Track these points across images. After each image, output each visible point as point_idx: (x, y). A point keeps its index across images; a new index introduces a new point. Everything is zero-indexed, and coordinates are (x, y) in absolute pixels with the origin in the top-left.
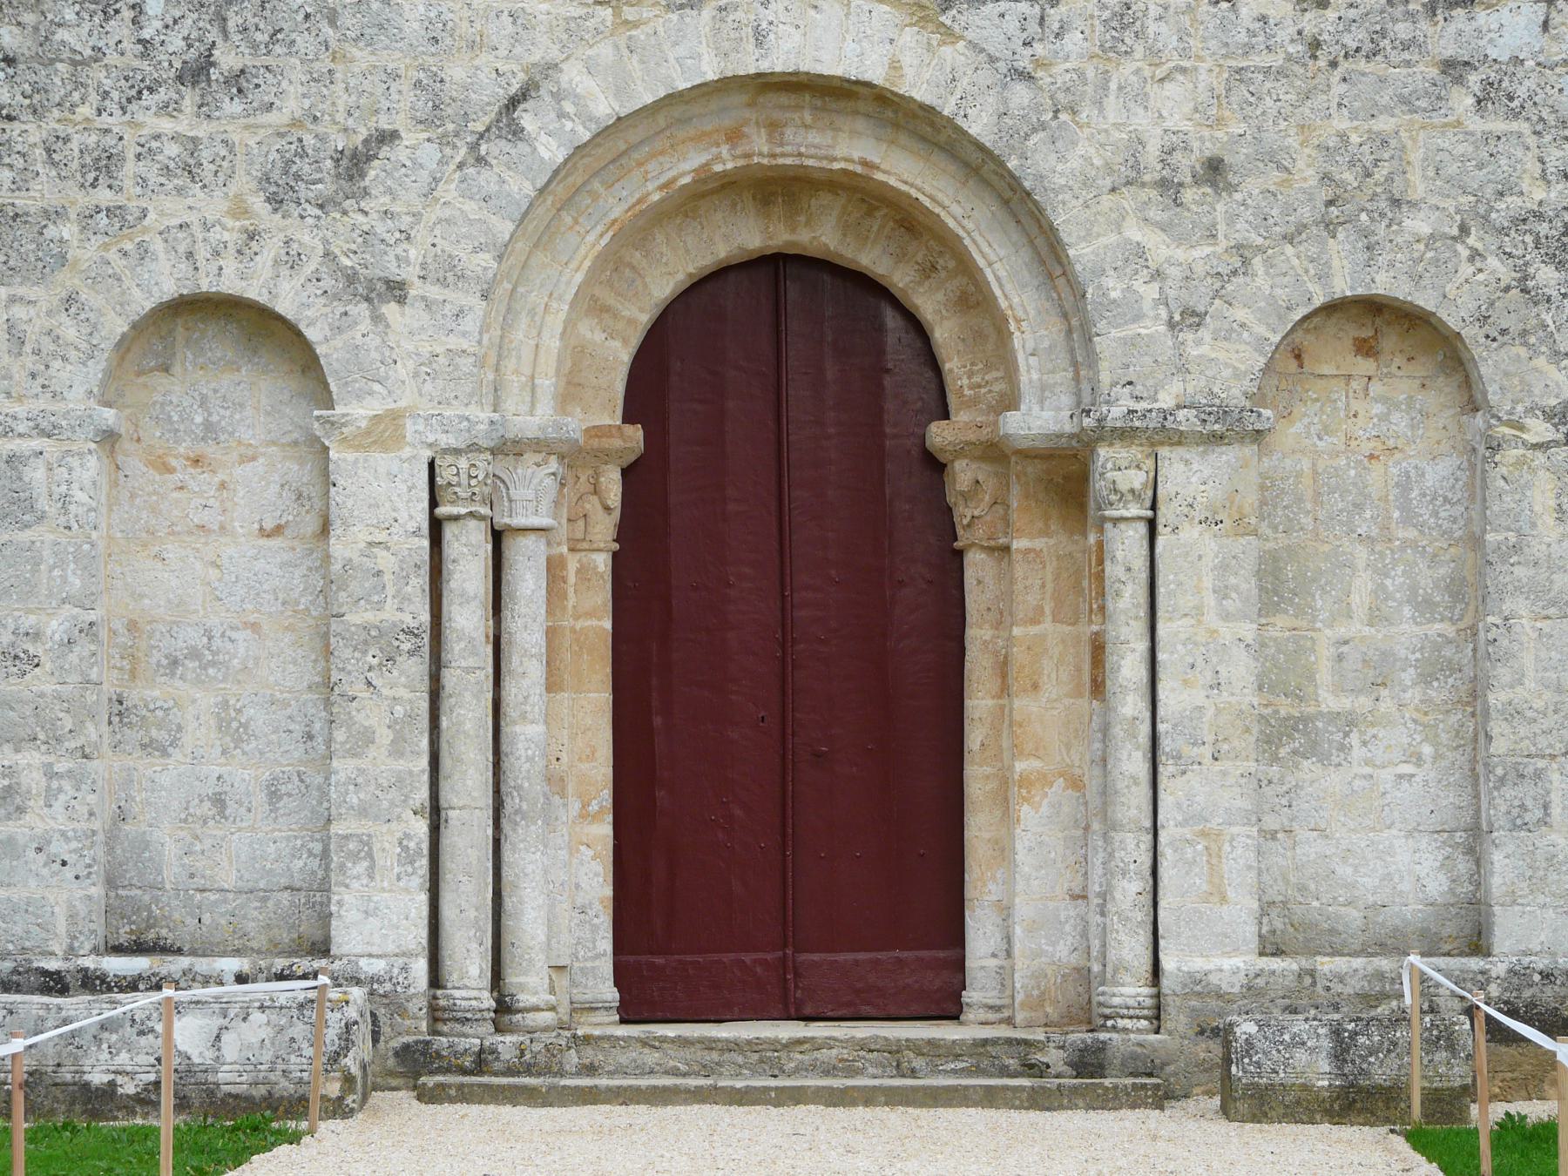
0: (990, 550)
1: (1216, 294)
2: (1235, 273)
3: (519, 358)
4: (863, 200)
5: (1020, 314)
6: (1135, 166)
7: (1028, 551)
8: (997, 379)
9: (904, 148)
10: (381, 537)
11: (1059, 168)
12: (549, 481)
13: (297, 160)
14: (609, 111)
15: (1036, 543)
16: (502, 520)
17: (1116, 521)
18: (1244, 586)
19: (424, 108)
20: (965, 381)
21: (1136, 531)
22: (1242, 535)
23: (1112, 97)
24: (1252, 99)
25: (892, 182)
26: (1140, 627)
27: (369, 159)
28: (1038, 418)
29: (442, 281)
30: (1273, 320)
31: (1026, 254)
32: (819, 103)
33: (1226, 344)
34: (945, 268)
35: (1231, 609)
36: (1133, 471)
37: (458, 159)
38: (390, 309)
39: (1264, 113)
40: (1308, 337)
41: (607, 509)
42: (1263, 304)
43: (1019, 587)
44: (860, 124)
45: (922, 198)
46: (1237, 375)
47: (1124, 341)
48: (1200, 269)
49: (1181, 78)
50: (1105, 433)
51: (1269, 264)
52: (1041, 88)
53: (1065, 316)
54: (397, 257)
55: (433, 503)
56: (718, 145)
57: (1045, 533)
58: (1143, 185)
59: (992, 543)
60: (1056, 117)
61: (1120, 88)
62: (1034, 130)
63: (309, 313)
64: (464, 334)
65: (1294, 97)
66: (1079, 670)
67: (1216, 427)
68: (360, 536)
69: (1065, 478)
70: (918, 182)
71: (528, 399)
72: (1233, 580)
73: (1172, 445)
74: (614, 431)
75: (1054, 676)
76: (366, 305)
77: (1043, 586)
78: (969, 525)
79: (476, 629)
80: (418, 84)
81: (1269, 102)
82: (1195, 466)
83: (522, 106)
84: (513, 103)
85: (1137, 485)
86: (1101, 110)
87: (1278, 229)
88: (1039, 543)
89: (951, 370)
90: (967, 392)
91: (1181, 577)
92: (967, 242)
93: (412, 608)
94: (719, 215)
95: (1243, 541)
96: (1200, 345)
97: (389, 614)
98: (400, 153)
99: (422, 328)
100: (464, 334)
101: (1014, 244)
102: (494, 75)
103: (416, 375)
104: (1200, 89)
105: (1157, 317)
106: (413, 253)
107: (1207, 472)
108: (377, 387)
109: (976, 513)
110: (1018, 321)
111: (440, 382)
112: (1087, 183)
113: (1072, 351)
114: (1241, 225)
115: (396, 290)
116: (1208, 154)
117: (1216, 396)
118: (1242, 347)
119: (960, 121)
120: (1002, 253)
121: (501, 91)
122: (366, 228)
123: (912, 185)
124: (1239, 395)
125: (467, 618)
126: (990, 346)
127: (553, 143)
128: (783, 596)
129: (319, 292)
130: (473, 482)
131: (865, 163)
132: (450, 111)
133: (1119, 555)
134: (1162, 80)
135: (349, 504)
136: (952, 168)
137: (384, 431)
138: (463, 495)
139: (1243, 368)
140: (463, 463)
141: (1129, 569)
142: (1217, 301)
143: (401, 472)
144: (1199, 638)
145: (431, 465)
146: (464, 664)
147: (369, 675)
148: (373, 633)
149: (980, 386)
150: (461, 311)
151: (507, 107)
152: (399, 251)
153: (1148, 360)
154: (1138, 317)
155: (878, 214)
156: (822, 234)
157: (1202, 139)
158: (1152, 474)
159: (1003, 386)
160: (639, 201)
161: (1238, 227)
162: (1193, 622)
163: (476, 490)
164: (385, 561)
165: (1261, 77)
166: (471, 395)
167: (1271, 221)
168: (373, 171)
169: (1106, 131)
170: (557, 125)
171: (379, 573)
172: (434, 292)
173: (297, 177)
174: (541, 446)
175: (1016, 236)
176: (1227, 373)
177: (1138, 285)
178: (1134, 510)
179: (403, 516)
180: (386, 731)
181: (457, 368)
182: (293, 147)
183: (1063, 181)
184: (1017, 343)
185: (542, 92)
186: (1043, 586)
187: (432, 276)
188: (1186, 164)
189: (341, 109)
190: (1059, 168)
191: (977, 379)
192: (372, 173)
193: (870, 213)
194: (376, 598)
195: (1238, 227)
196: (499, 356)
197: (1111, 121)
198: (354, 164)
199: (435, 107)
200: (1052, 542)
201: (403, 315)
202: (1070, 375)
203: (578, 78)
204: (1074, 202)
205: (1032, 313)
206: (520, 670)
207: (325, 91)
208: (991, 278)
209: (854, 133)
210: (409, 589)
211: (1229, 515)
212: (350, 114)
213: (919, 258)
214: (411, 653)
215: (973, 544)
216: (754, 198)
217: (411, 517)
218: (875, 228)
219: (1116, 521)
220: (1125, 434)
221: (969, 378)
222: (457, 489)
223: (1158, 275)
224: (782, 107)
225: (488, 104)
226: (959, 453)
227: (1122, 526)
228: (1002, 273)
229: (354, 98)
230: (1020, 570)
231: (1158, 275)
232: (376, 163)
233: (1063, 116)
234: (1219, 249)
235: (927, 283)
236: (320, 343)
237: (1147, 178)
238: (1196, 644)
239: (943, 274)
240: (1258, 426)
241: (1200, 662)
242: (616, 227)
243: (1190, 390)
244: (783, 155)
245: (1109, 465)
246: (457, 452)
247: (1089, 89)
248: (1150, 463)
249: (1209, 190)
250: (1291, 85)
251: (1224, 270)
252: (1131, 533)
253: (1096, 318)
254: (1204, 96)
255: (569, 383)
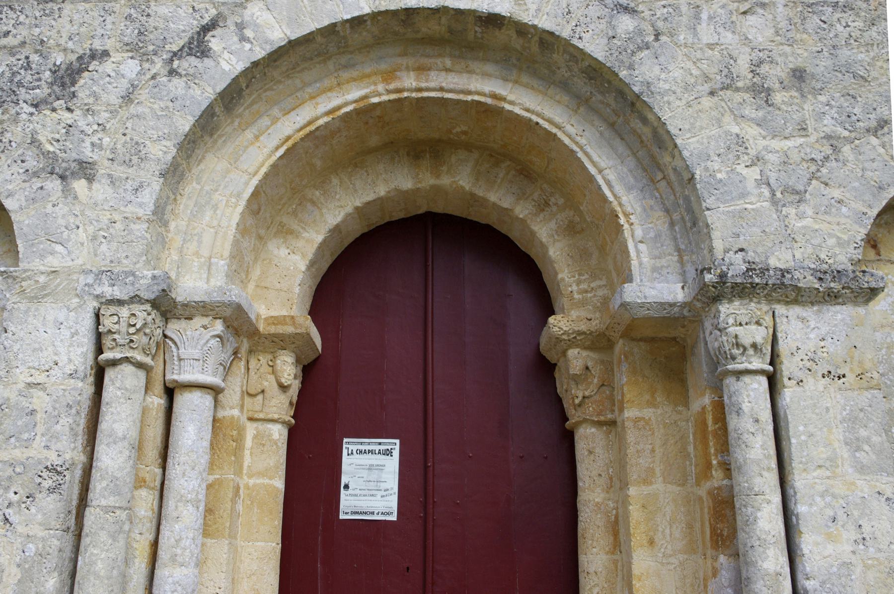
0: (600, 424)
1: (813, 176)
2: (827, 158)
3: (200, 242)
4: (491, 156)
5: (629, 209)
6: (730, 74)
7: (637, 420)
8: (600, 287)
9: (526, 86)
10: (40, 378)
11: (663, 76)
12: (214, 342)
13: (22, 72)
14: (282, 35)
15: (647, 417)
16: (174, 376)
17: (739, 374)
18: (876, 439)
19: (130, 34)
20: (575, 288)
21: (760, 384)
22: (867, 389)
23: (704, 25)
24: (825, 26)
25: (517, 110)
26: (772, 478)
27: (80, 71)
28: (654, 284)
29: (128, 163)
30: (868, 197)
31: (631, 162)
32: (457, 53)
33: (828, 218)
34: (556, 204)
35: (865, 462)
36: (754, 327)
37: (154, 71)
38: (79, 185)
39: (836, 36)
40: (881, 230)
41: (283, 388)
42: (856, 184)
43: (631, 451)
44: (489, 68)
45: (541, 122)
46: (840, 243)
47: (733, 215)
48: (795, 157)
49: (760, 11)
50: (715, 292)
51: (857, 151)
52: (643, 19)
53: (667, 211)
54: (93, 144)
55: (99, 350)
56: (375, 84)
57: (652, 404)
58: (738, 89)
59: (602, 418)
60: (657, 39)
61: (710, 18)
62: (640, 49)
63: (10, 187)
64: (141, 205)
65: (862, 24)
66: (690, 526)
67: (832, 285)
68: (22, 377)
69: (673, 349)
70: (539, 109)
71: (205, 276)
72: (863, 433)
73: (787, 303)
74: (287, 320)
75: (668, 531)
76: (59, 181)
77: (653, 451)
78: (580, 405)
79: (121, 469)
80: (129, 17)
81: (840, 28)
82: (812, 324)
83: (211, 33)
84: (206, 29)
85: (759, 340)
86: (695, 34)
87: (861, 124)
88: (648, 413)
89: (563, 279)
90: (576, 296)
91: (811, 428)
92: (580, 155)
93: (59, 446)
94: (381, 167)
95: (868, 394)
96: (801, 219)
97: (37, 451)
98: (108, 67)
99: (106, 200)
100: (141, 205)
101: (620, 156)
102: (191, 10)
103: (94, 238)
104: (779, 19)
105: (760, 195)
106: (106, 140)
107: (824, 330)
108: (59, 248)
109: (587, 394)
110: (627, 215)
111: (115, 245)
112: (687, 88)
113: (675, 239)
114: (827, 120)
115: (85, 170)
116: (791, 66)
117: (824, 262)
118: (843, 220)
119: (575, 42)
120: (611, 163)
121: (195, 22)
122: (69, 122)
123: (533, 112)
124: (846, 261)
125: (112, 459)
126: (594, 262)
127: (234, 60)
128: (426, 467)
129: (21, 171)
130: (132, 330)
131: (494, 96)
132: (152, 36)
133: (746, 407)
134: (744, 13)
135: (16, 348)
136: (566, 98)
137: (59, 285)
138: (121, 341)
139: (845, 237)
140: (124, 312)
141: (757, 421)
142: (814, 182)
143: (67, 319)
144: (837, 491)
145: (97, 316)
146: (104, 503)
147: (7, 511)
148: (18, 470)
149: (586, 292)
150: (141, 186)
151: (198, 33)
152: (95, 139)
153: (757, 230)
154: (743, 195)
155: (503, 165)
156: (459, 184)
157: (785, 55)
158: (771, 331)
159: (606, 292)
160: (310, 123)
161: (825, 122)
162: (828, 473)
163: (134, 338)
164: (40, 401)
165: (830, 9)
166: (140, 255)
167: (854, 118)
168: (84, 80)
169: (701, 49)
170: (238, 46)
171: (33, 412)
172: (119, 171)
173: (20, 84)
174: (204, 309)
175: (621, 148)
176: (831, 242)
177: (740, 169)
178: (758, 363)
179: (63, 359)
180: (14, 570)
181: (131, 232)
182: (21, 62)
183: (667, 86)
184: (627, 233)
185: (229, 22)
186: (653, 451)
187: (120, 158)
188: (774, 73)
189: (64, 35)
190: (663, 76)
191: (584, 286)
192: (82, 82)
193: (497, 164)
194: (25, 436)
195: (825, 122)
196: (184, 240)
197: (705, 42)
198: (67, 78)
199: (140, 33)
200: (659, 411)
201: (90, 189)
202: (676, 258)
203: (259, 13)
204: (678, 103)
205: (639, 210)
206: (175, 514)
207: (53, 23)
208: (601, 182)
209: (485, 75)
210: (58, 427)
211: (851, 370)
212: (70, 39)
213: (536, 196)
214: (51, 490)
215: (585, 421)
216: (408, 154)
217: (70, 360)
218: (501, 175)
219: (739, 374)
220: (744, 290)
221: (578, 285)
222: (116, 336)
223: (757, 160)
224: (428, 56)
225: (184, 31)
226: (572, 343)
227: (747, 379)
228: (612, 177)
229: (75, 27)
230: (631, 436)
231: (757, 160)
232: (86, 74)
233: (663, 38)
234: (812, 139)
235: (542, 215)
236: (16, 212)
237: (740, 84)
238: (834, 496)
239: (555, 209)
240: (873, 285)
241: (841, 514)
242: (290, 143)
243: (798, 255)
244: (428, 89)
245: (731, 321)
246: (120, 303)
247: (684, 19)
248: (768, 320)
249: (796, 94)
250: (857, 15)
251: (819, 157)
252: (755, 386)
253: (706, 195)
254: (783, 24)
255: (257, 286)
